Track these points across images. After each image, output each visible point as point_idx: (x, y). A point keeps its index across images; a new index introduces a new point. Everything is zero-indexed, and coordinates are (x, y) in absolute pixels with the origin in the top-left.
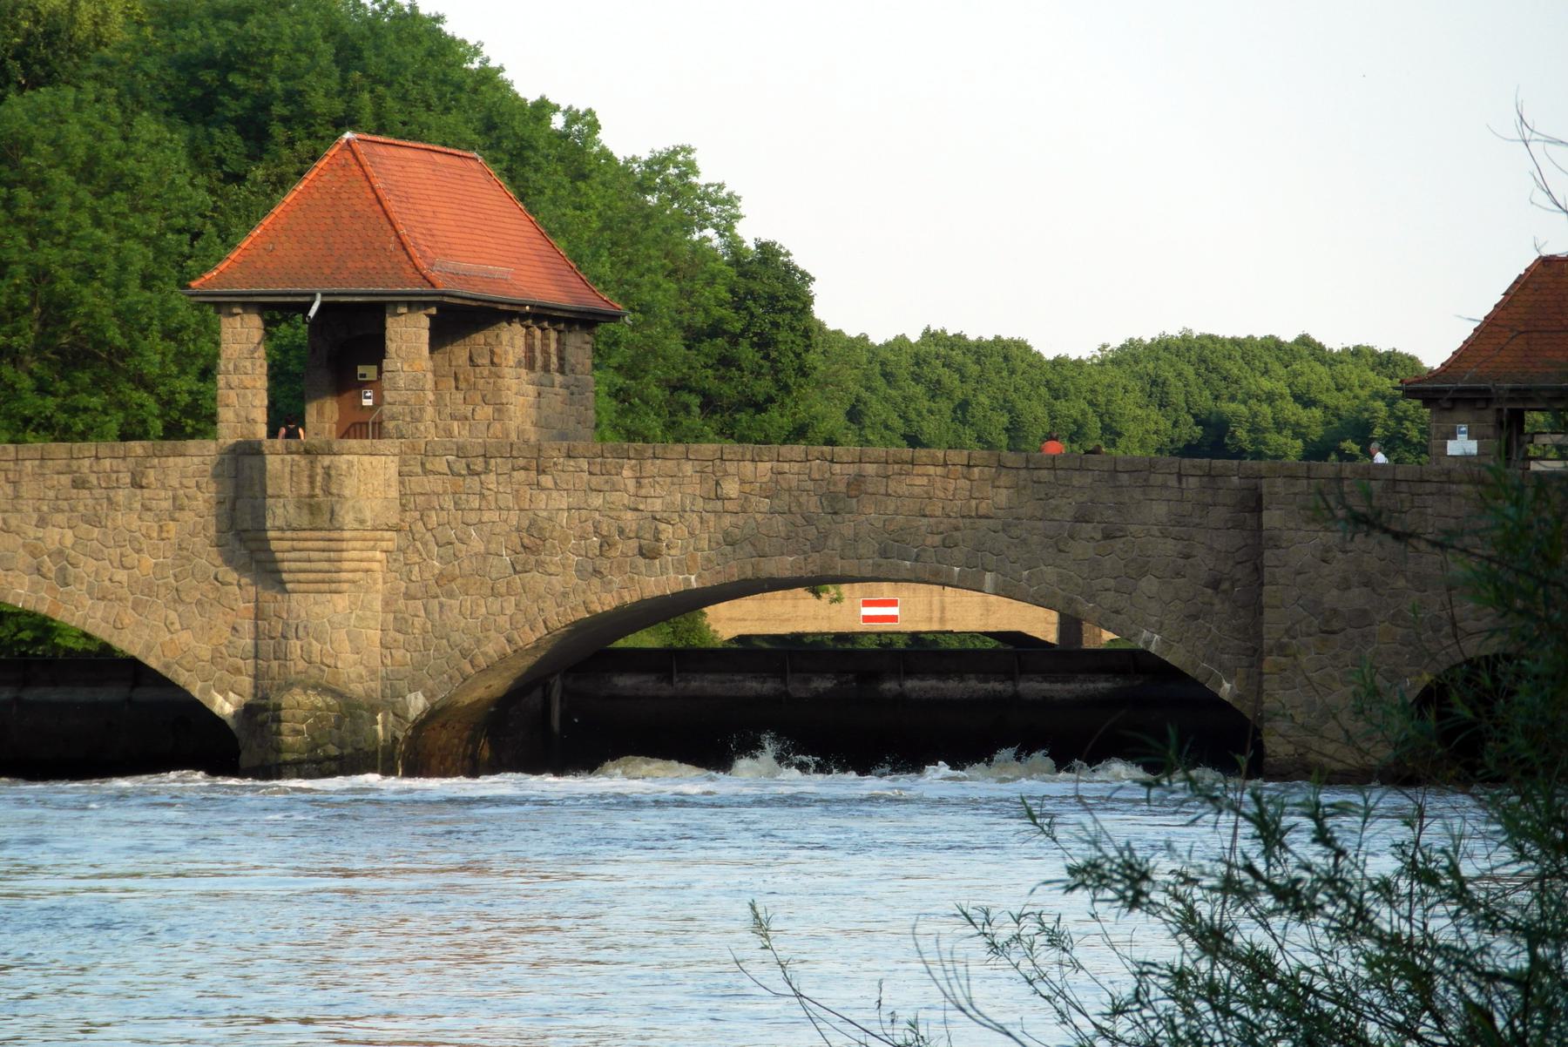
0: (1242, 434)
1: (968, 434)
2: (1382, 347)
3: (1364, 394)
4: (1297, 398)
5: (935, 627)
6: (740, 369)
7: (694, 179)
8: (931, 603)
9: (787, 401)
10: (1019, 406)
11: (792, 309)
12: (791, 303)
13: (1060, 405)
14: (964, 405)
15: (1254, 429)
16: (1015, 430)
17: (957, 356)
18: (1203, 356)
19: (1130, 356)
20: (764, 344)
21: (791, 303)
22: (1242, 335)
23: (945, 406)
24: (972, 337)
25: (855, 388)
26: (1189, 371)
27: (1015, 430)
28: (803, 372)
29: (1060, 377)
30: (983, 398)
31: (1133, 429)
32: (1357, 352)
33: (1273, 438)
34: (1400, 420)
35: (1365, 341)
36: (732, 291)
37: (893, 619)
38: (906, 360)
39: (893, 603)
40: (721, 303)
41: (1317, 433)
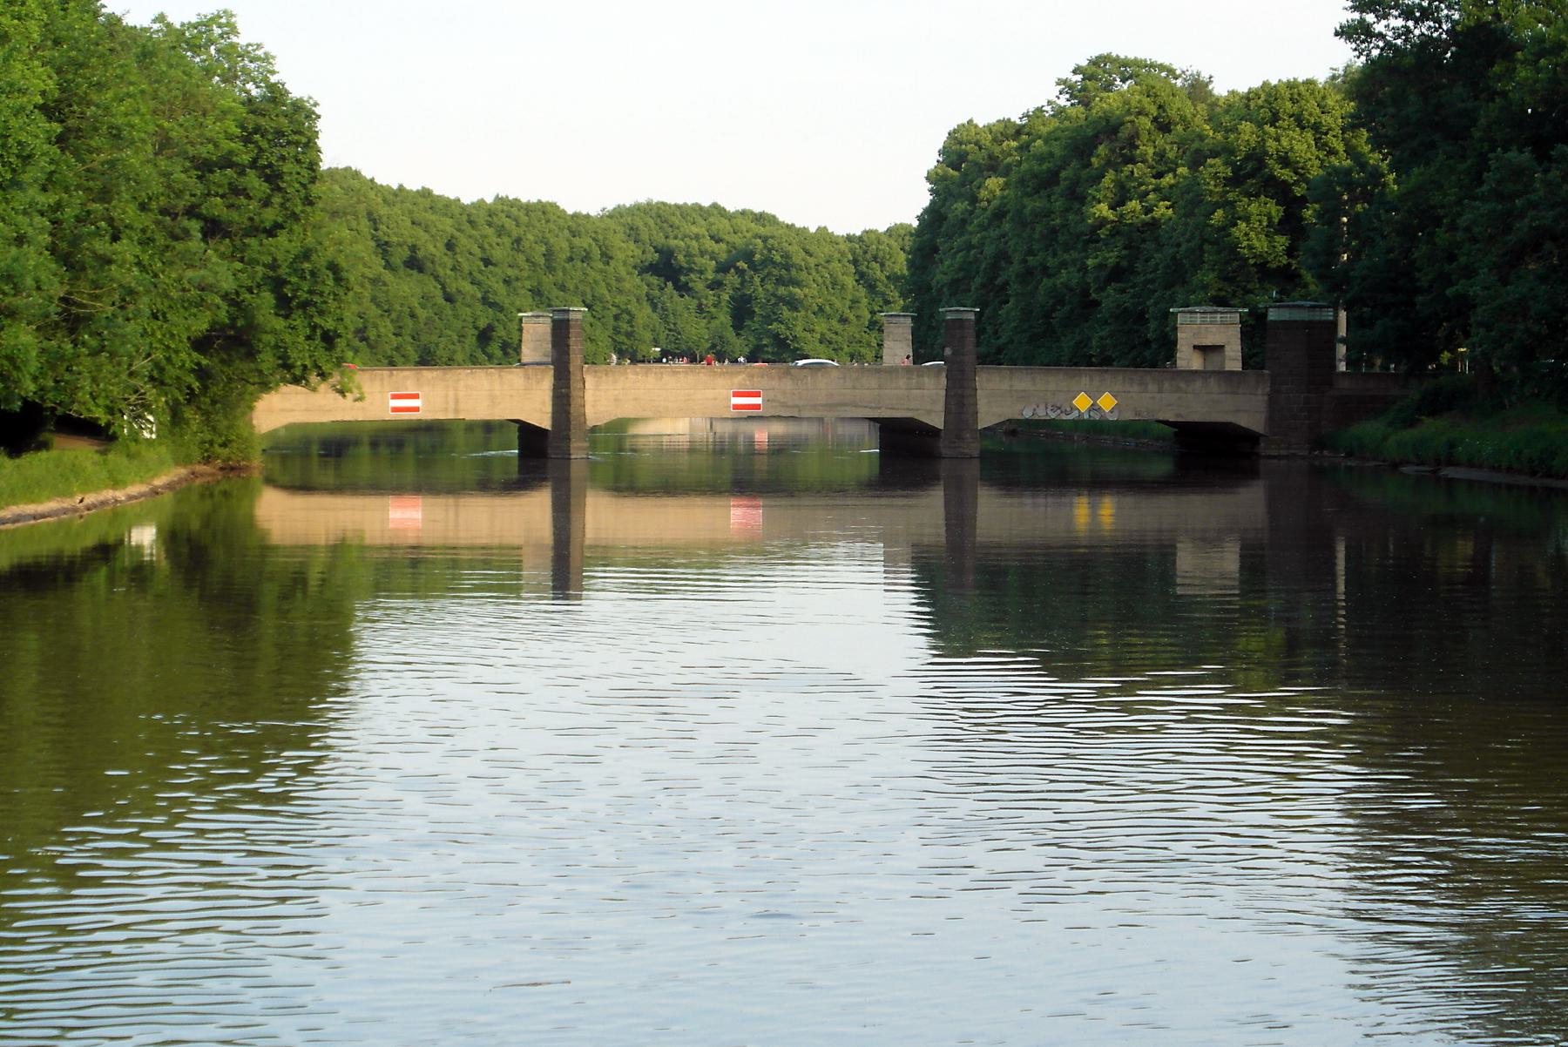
0: (681, 257)
1: (521, 258)
2: (757, 210)
3: (748, 235)
4: (712, 238)
5: (451, 416)
6: (249, 197)
7: (234, 39)
8: (446, 396)
9: (295, 227)
10: (551, 241)
11: (297, 144)
12: (296, 137)
13: (576, 241)
14: (518, 241)
15: (688, 255)
16: (549, 255)
17: (514, 211)
18: (659, 214)
19: (618, 214)
20: (273, 177)
21: (296, 137)
22: (681, 202)
23: (507, 241)
24: (524, 200)
25: (450, 230)
26: (651, 222)
27: (549, 255)
28: (309, 201)
29: (578, 224)
30: (530, 237)
31: (620, 256)
32: (743, 213)
33: (698, 260)
34: (770, 251)
35: (748, 207)
36: (243, 128)
37: (416, 409)
38: (483, 214)
39: (416, 396)
40: (231, 138)
41: (723, 257)
